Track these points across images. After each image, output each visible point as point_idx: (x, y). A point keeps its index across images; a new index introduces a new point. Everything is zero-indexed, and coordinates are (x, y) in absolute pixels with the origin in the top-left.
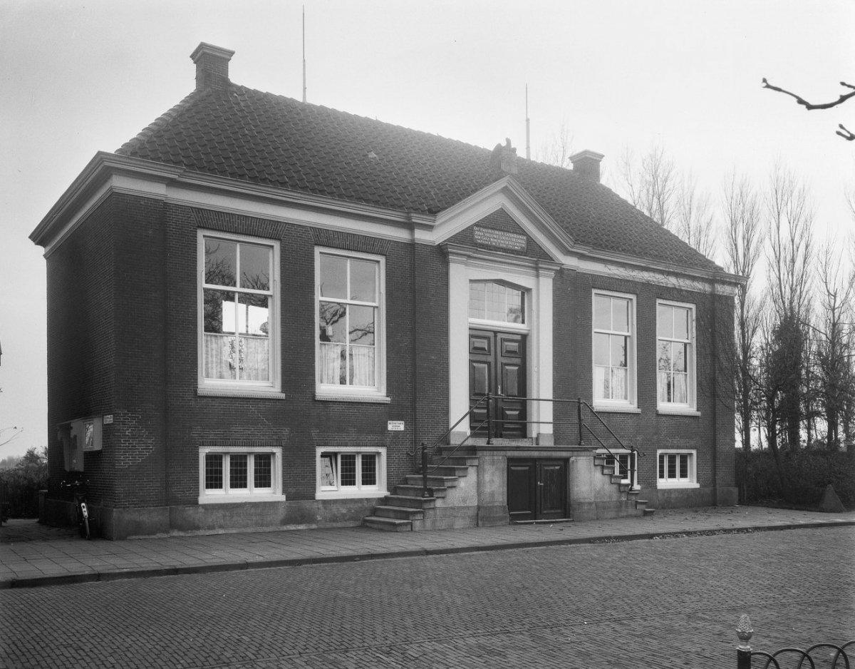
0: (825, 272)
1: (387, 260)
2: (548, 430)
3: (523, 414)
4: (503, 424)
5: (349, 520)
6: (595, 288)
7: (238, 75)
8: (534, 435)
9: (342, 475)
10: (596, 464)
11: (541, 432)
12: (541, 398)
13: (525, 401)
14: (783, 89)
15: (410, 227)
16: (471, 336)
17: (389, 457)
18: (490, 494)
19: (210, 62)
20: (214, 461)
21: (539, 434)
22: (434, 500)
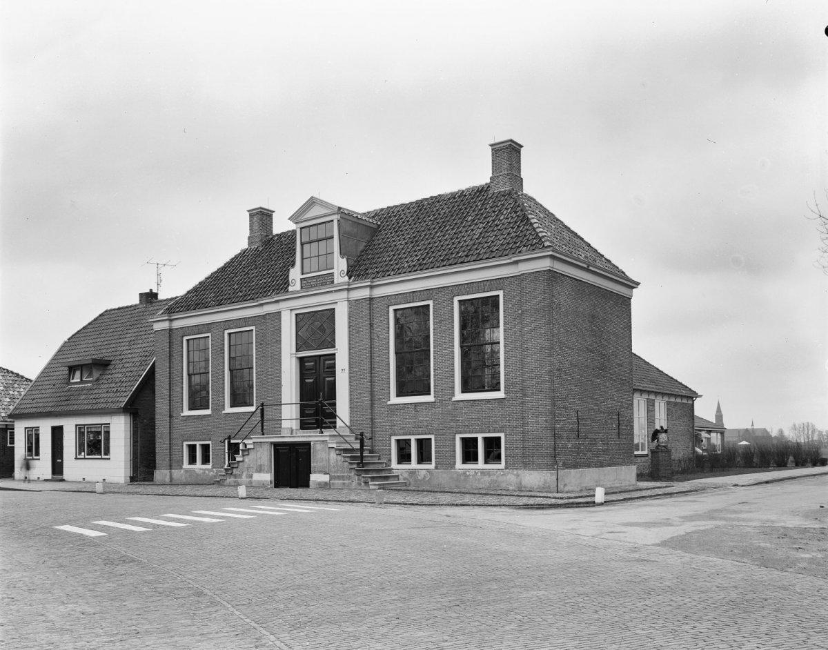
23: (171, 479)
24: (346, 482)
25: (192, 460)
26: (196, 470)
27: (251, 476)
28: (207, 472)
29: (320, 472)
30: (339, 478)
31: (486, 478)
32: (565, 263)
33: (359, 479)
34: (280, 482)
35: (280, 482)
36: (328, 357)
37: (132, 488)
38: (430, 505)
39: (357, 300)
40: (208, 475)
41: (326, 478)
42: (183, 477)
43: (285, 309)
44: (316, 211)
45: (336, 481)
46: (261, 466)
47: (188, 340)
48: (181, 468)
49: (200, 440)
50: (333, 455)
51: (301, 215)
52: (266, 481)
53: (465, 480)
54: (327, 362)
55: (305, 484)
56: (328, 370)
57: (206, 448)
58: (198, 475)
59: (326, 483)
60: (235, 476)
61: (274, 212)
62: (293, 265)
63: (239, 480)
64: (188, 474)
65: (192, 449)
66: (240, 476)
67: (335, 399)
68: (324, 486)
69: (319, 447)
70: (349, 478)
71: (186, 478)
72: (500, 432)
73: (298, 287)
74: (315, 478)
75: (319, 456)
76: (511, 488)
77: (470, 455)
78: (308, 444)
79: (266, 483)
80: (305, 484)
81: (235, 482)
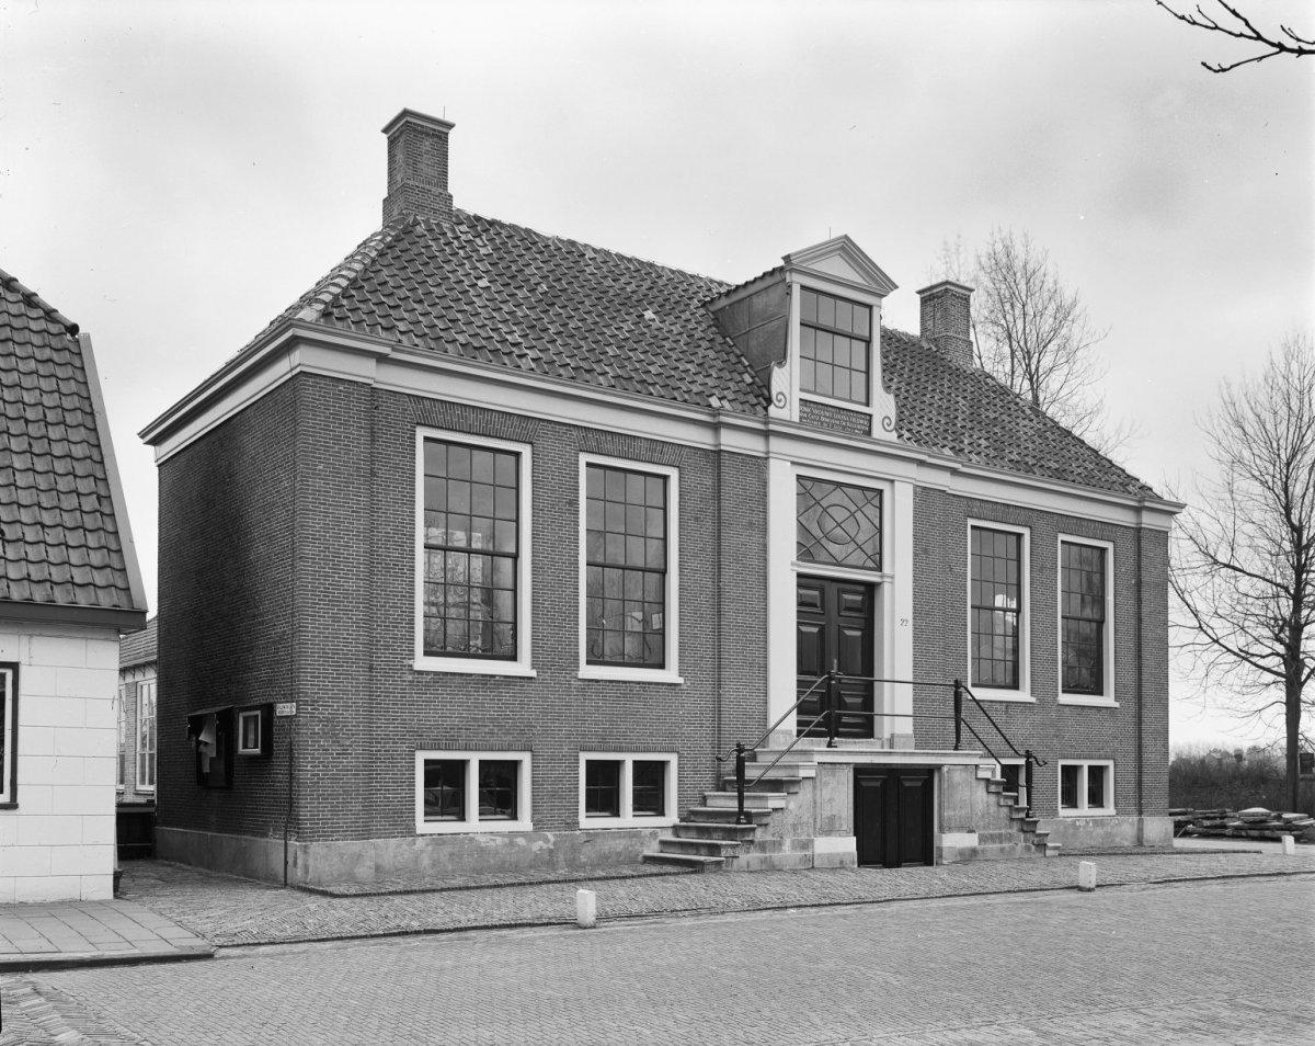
0: (1286, 490)
1: (680, 474)
2: (905, 727)
3: (868, 702)
4: (840, 716)
5: (623, 863)
6: (972, 517)
7: (477, 184)
8: (887, 735)
9: (587, 790)
10: (979, 776)
11: (897, 732)
12: (896, 679)
13: (872, 683)
14: (1034, 791)
15: (716, 427)
16: (799, 586)
17: (534, 768)
18: (828, 818)
19: (417, 142)
20: (1070, 773)
21: (893, 736)
22: (753, 830)
23: (1140, 841)
24: (1006, 845)
25: (1070, 799)
26: (478, 838)
27: (806, 845)
28: (521, 841)
29: (960, 828)
30: (992, 838)
31: (1100, 831)
32: (529, 391)
33: (1025, 841)
34: (871, 854)
35: (871, 854)
36: (848, 587)
37: (156, 922)
38: (385, 935)
39: (925, 488)
40: (524, 850)
41: (970, 841)
42: (426, 862)
43: (782, 457)
44: (837, 267)
45: (990, 846)
46: (832, 819)
47: (1019, 536)
48: (410, 831)
49: (637, 750)
50: (980, 792)
51: (812, 259)
52: (849, 854)
53: (1074, 835)
54: (846, 596)
55: (925, 854)
56: (848, 614)
57: (1097, 774)
58: (482, 851)
59: (974, 851)
60: (763, 847)
61: (451, 126)
62: (782, 359)
63: (776, 856)
64: (447, 849)
65: (1070, 773)
66: (778, 845)
67: (798, 681)
68: (969, 856)
69: (958, 776)
70: (1010, 838)
71: (434, 864)
72: (577, 760)
73: (793, 412)
74: (951, 841)
75: (958, 797)
76: (1126, 844)
77: (603, 797)
78: (929, 772)
79: (847, 860)
80: (925, 854)
81: (764, 861)
